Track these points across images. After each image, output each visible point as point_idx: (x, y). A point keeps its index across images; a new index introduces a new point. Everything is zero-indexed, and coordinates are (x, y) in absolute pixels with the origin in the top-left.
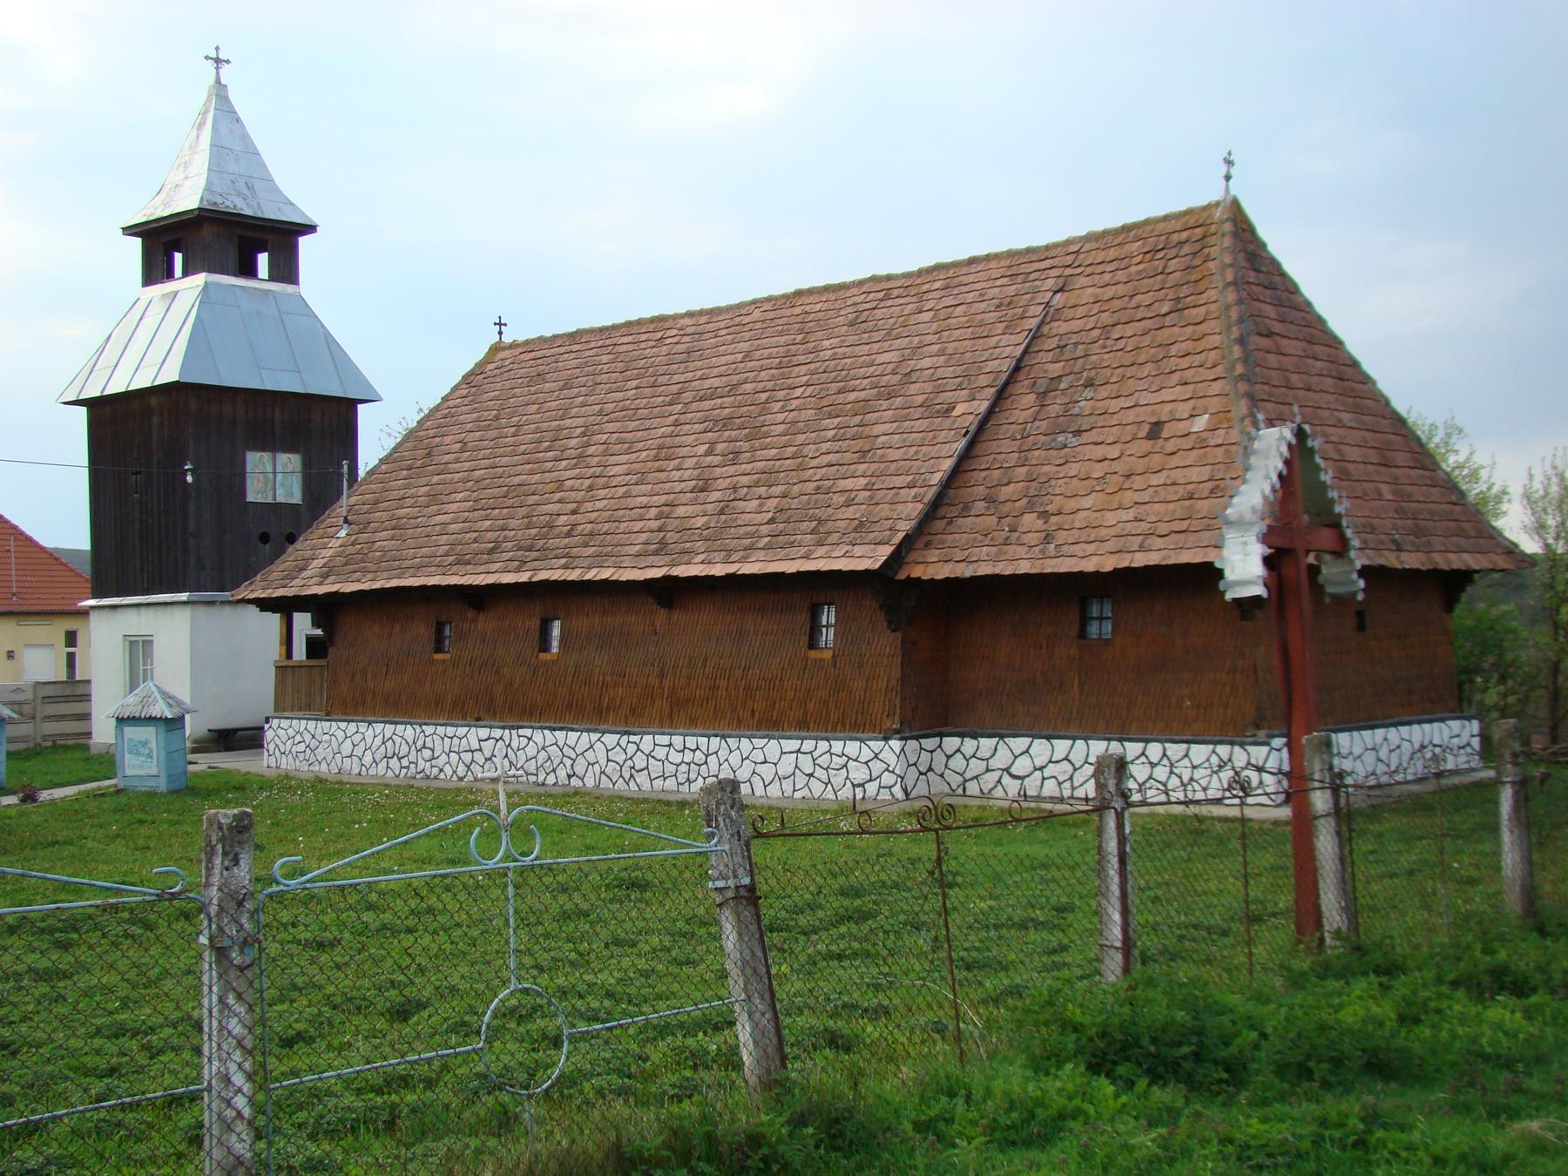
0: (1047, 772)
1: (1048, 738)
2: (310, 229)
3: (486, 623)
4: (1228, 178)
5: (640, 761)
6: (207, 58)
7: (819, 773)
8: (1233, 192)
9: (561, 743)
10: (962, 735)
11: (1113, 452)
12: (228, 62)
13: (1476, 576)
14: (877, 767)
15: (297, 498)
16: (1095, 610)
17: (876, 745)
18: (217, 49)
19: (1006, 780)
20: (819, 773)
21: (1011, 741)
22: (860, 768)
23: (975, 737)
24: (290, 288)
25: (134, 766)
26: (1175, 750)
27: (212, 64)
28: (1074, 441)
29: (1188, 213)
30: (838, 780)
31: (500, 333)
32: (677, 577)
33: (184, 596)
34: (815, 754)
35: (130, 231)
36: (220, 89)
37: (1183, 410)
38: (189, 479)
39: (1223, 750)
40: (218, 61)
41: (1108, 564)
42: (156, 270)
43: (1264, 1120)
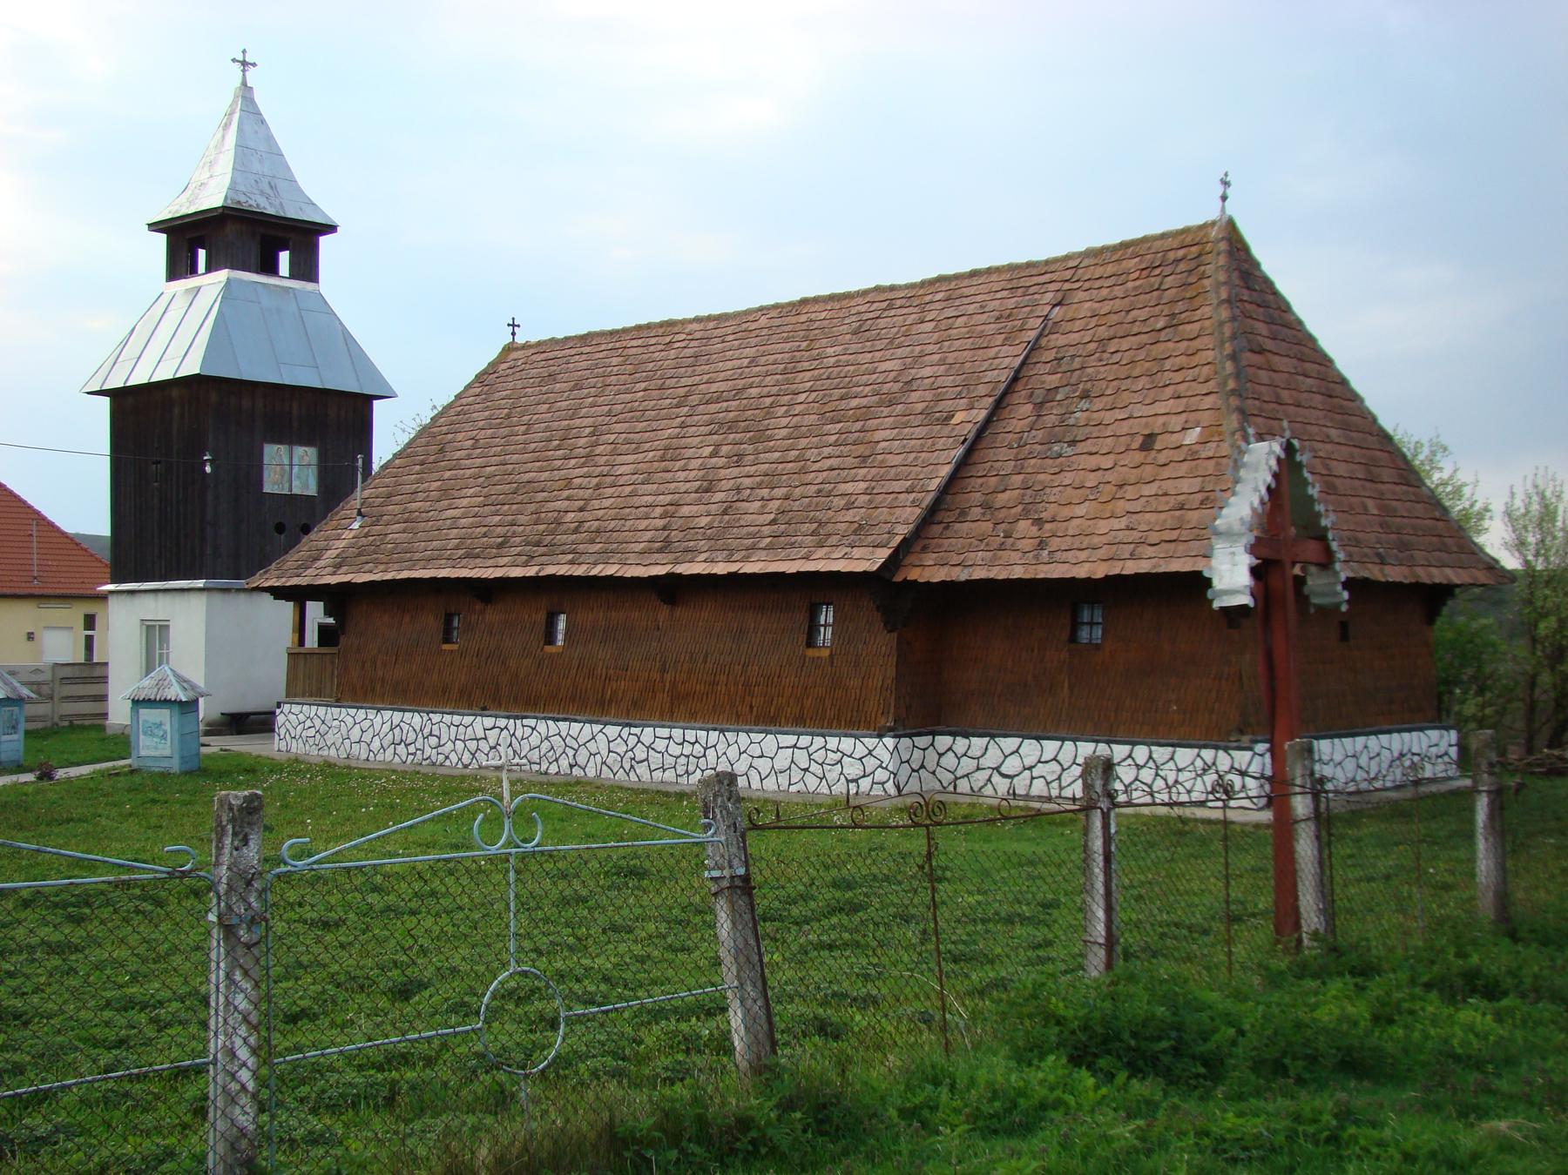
0: (1036, 772)
1: (1038, 739)
2: (331, 229)
3: (493, 615)
4: (1224, 198)
5: (640, 753)
6: (234, 60)
7: (814, 767)
8: (1229, 212)
9: (564, 734)
10: (954, 734)
11: (1107, 462)
12: (254, 65)
14: (871, 763)
15: (312, 490)
17: (871, 742)
18: (244, 52)
19: (996, 778)
20: (814, 767)
22: (851, 765)
24: (309, 286)
25: (148, 747)
26: (1161, 753)
27: (238, 68)
30: (833, 774)
31: (513, 334)
33: (200, 583)
34: (811, 750)
36: (246, 91)
37: (1176, 422)
38: (208, 469)
39: (1208, 754)
40: (244, 63)
41: (1100, 571)
43: (1240, 1115)
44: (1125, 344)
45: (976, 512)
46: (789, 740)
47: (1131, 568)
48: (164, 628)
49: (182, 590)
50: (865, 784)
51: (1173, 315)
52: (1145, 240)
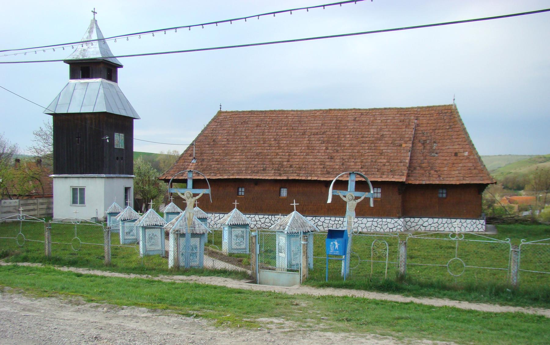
1: (433, 218)
2: (121, 66)
5: (320, 223)
7: (379, 226)
10: (410, 218)
11: (448, 158)
13: (489, 186)
14: (396, 224)
15: (123, 148)
16: (240, 190)
17: (396, 220)
19: (422, 227)
20: (379, 226)
21: (423, 219)
23: (414, 218)
27: (92, 13)
28: (436, 155)
29: (445, 106)
32: (411, 184)
33: (104, 175)
35: (66, 61)
37: (462, 150)
38: (108, 141)
39: (474, 221)
41: (458, 183)
42: (73, 75)
44: (440, 131)
45: (418, 168)
46: (372, 219)
47: (464, 182)
48: (82, 190)
49: (101, 177)
50: (395, 229)
51: (450, 126)
52: (434, 106)
